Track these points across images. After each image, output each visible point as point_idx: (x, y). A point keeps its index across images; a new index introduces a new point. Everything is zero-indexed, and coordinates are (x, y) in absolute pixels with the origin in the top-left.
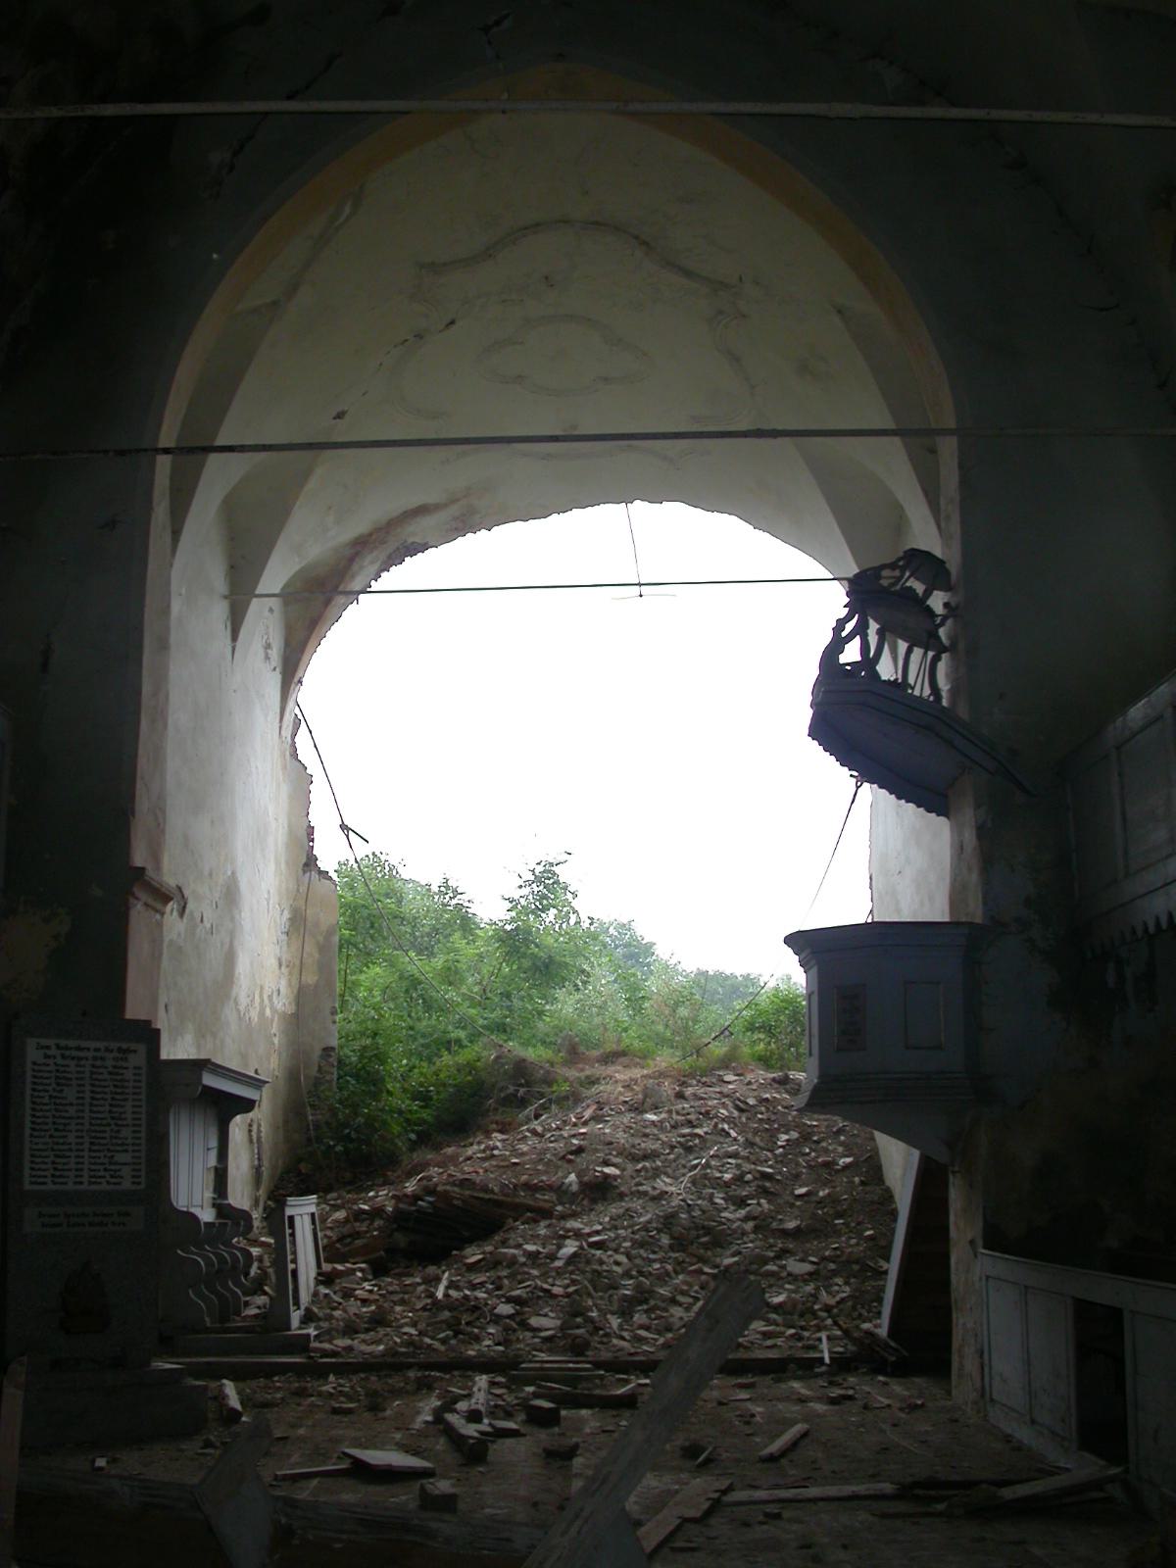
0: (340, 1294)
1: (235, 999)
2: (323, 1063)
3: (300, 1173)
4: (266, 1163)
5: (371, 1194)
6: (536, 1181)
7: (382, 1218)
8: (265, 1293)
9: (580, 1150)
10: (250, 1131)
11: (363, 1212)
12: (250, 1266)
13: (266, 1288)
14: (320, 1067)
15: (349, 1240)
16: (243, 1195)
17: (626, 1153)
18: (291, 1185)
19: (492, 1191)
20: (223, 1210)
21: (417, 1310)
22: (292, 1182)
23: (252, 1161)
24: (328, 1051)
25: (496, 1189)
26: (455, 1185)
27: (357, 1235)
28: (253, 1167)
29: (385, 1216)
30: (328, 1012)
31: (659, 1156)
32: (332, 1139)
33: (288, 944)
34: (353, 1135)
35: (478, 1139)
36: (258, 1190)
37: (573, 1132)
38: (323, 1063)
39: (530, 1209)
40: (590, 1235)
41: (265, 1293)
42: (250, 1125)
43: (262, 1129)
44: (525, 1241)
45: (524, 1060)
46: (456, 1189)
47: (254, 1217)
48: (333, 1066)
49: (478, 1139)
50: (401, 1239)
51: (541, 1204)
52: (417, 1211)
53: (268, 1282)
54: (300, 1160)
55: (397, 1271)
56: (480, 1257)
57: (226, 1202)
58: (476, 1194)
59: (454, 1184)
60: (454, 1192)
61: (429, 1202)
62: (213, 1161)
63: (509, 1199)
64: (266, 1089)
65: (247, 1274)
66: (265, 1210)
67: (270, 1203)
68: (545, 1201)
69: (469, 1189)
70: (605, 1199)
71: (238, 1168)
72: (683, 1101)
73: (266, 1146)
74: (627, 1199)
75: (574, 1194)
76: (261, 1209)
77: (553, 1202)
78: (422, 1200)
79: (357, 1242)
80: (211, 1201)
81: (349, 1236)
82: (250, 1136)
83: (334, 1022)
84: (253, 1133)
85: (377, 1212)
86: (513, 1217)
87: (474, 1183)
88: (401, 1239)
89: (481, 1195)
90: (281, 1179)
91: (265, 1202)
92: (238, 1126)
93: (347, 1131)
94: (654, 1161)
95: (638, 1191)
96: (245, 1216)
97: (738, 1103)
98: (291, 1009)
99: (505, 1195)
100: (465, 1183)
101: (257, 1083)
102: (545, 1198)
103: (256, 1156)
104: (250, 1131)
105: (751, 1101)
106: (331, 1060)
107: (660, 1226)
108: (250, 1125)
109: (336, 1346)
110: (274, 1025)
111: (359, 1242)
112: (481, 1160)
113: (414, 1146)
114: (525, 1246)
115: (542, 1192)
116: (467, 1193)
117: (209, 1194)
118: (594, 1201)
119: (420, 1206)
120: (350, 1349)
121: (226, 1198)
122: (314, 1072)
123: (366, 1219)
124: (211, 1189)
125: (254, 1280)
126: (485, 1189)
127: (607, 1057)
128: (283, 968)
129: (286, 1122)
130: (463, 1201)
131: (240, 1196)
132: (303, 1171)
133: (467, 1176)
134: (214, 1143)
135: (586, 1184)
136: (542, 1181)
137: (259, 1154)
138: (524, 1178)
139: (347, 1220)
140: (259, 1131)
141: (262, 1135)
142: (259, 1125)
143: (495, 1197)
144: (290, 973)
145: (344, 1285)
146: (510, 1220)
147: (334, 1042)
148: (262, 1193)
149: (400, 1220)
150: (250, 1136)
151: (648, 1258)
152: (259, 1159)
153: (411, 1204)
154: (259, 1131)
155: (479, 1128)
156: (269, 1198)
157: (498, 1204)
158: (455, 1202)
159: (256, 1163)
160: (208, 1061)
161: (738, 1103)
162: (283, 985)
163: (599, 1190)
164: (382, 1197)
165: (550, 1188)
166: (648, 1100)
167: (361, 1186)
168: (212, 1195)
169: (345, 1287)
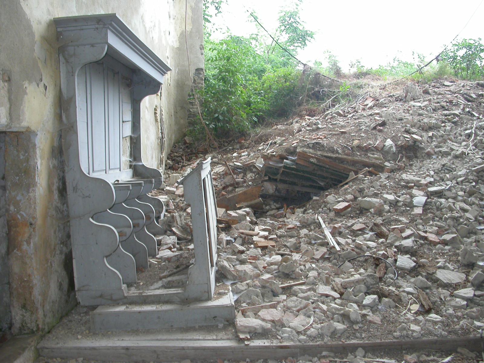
0: (240, 240)
1: (142, 17)
2: (196, 78)
3: (185, 143)
4: (166, 132)
5: (235, 154)
6: (365, 144)
7: (251, 171)
8: (174, 234)
9: (383, 124)
10: (155, 113)
11: (238, 167)
12: (160, 212)
13: (174, 229)
14: (194, 80)
15: (230, 188)
16: (152, 158)
17: (418, 126)
18: (181, 150)
19: (337, 152)
20: (138, 171)
21: (318, 260)
22: (181, 148)
23: (157, 134)
24: (199, 71)
25: (340, 151)
26: (310, 148)
27: (236, 185)
28: (158, 138)
29: (254, 170)
30: (198, 48)
31: (440, 128)
32: (207, 120)
33: (174, 5)
34: (221, 118)
35: (296, 120)
36: (162, 153)
37: (370, 113)
38: (196, 78)
39: (366, 165)
40: (427, 185)
41: (174, 234)
42: (155, 110)
43: (163, 113)
44: (380, 192)
45: (319, 74)
46: (311, 150)
47: (160, 171)
48: (202, 80)
49: (296, 120)
50: (270, 188)
51: (374, 161)
52: (285, 167)
53: (175, 224)
54: (185, 135)
55: (272, 212)
56: (346, 204)
57: (141, 164)
58: (326, 154)
59: (308, 146)
60: (310, 152)
61: (292, 161)
62: (128, 131)
63: (350, 157)
64: (168, 75)
65: (158, 218)
66: (166, 166)
67: (169, 161)
68: (376, 158)
69: (319, 150)
70: (417, 157)
71: (148, 138)
72: (429, 96)
73: (165, 126)
74: (434, 157)
75: (394, 153)
76: (164, 166)
77: (381, 159)
78: (287, 159)
79: (237, 190)
80: (128, 163)
81: (231, 185)
82: (156, 117)
83: (202, 54)
84: (157, 115)
85: (248, 168)
86: (354, 171)
87: (323, 146)
88: (270, 188)
89: (330, 155)
90: (174, 146)
91: (166, 161)
92: (148, 103)
93: (217, 115)
94: (439, 131)
95: (440, 152)
96: (155, 174)
97: (465, 96)
98: (176, 45)
99: (347, 155)
100: (317, 146)
101: (163, 69)
102: (375, 157)
103: (160, 131)
104: (155, 113)
105: (474, 96)
106: (201, 76)
107: (475, 178)
108: (155, 110)
109: (263, 320)
110: (168, 51)
111: (239, 190)
112: (301, 133)
113: (255, 125)
114: (385, 196)
115: (372, 152)
116: (319, 153)
117: (126, 158)
118: (410, 158)
119: (285, 163)
120: (279, 324)
121: (140, 161)
122: (191, 83)
123: (240, 173)
124: (128, 154)
125: (164, 223)
126: (333, 151)
127: (359, 75)
128: (172, 19)
129: (176, 112)
130: (317, 159)
131: (151, 159)
132: (188, 142)
133: (315, 141)
134: (128, 117)
135: (402, 147)
136: (370, 144)
137: (162, 129)
138: (356, 142)
139: (226, 174)
140: (161, 114)
141: (164, 117)
142: (161, 111)
143: (340, 156)
144: (175, 23)
145: (241, 231)
146: (352, 173)
147: (202, 66)
148: (164, 155)
149: (270, 173)
150: (156, 117)
151: (480, 204)
152: (162, 133)
153: (277, 162)
154: (161, 114)
155: (295, 114)
156: (168, 158)
157: (342, 161)
158: (312, 160)
159: (160, 135)
160: (113, 18)
161: (465, 96)
162: (172, 29)
163: (411, 151)
164: (242, 157)
165: (377, 149)
166: (409, 94)
167: (226, 149)
168: (129, 159)
169: (242, 233)
